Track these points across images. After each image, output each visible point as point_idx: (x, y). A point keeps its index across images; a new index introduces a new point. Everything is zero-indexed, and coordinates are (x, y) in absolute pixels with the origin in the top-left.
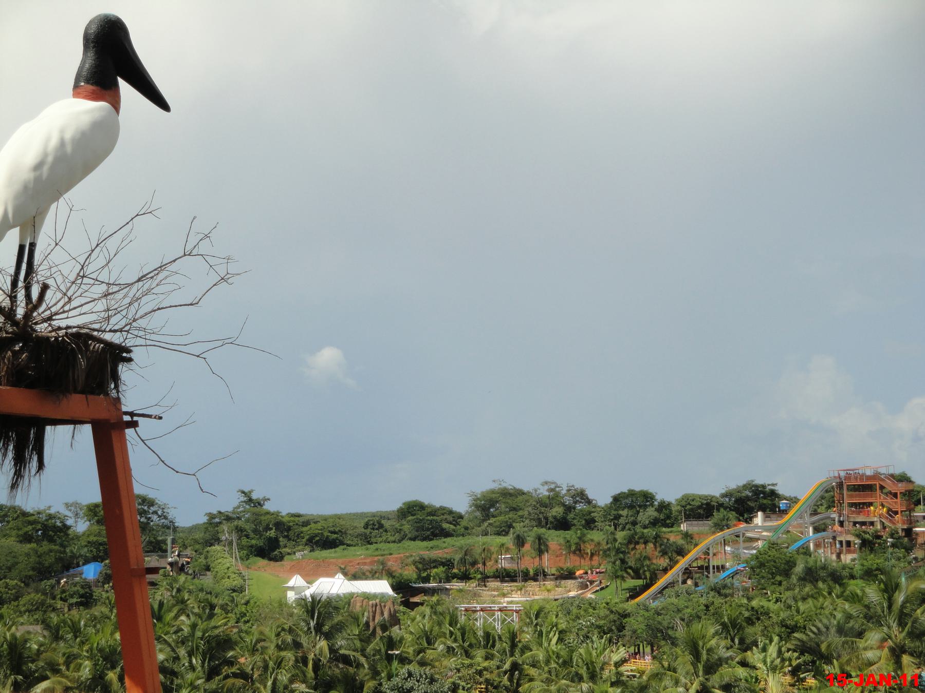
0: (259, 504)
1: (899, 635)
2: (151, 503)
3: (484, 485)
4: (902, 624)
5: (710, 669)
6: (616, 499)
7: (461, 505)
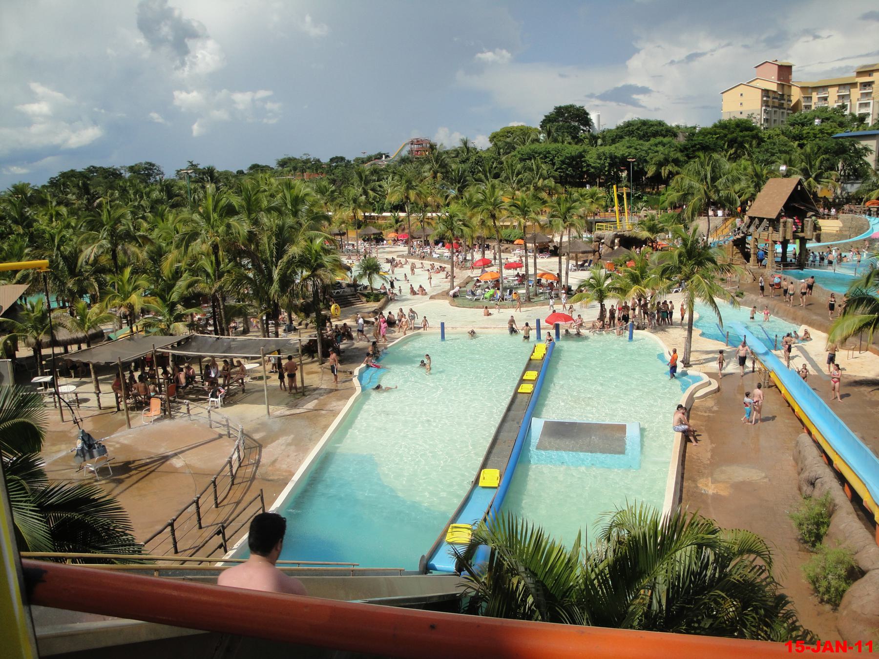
0: (195, 166)
1: (436, 166)
2: (154, 165)
3: (281, 157)
4: (437, 163)
5: (367, 182)
6: (332, 160)
7: (273, 164)
